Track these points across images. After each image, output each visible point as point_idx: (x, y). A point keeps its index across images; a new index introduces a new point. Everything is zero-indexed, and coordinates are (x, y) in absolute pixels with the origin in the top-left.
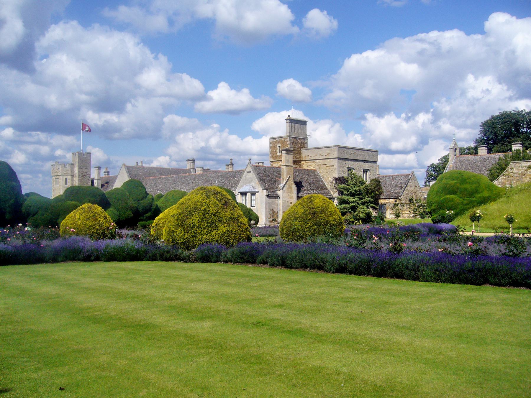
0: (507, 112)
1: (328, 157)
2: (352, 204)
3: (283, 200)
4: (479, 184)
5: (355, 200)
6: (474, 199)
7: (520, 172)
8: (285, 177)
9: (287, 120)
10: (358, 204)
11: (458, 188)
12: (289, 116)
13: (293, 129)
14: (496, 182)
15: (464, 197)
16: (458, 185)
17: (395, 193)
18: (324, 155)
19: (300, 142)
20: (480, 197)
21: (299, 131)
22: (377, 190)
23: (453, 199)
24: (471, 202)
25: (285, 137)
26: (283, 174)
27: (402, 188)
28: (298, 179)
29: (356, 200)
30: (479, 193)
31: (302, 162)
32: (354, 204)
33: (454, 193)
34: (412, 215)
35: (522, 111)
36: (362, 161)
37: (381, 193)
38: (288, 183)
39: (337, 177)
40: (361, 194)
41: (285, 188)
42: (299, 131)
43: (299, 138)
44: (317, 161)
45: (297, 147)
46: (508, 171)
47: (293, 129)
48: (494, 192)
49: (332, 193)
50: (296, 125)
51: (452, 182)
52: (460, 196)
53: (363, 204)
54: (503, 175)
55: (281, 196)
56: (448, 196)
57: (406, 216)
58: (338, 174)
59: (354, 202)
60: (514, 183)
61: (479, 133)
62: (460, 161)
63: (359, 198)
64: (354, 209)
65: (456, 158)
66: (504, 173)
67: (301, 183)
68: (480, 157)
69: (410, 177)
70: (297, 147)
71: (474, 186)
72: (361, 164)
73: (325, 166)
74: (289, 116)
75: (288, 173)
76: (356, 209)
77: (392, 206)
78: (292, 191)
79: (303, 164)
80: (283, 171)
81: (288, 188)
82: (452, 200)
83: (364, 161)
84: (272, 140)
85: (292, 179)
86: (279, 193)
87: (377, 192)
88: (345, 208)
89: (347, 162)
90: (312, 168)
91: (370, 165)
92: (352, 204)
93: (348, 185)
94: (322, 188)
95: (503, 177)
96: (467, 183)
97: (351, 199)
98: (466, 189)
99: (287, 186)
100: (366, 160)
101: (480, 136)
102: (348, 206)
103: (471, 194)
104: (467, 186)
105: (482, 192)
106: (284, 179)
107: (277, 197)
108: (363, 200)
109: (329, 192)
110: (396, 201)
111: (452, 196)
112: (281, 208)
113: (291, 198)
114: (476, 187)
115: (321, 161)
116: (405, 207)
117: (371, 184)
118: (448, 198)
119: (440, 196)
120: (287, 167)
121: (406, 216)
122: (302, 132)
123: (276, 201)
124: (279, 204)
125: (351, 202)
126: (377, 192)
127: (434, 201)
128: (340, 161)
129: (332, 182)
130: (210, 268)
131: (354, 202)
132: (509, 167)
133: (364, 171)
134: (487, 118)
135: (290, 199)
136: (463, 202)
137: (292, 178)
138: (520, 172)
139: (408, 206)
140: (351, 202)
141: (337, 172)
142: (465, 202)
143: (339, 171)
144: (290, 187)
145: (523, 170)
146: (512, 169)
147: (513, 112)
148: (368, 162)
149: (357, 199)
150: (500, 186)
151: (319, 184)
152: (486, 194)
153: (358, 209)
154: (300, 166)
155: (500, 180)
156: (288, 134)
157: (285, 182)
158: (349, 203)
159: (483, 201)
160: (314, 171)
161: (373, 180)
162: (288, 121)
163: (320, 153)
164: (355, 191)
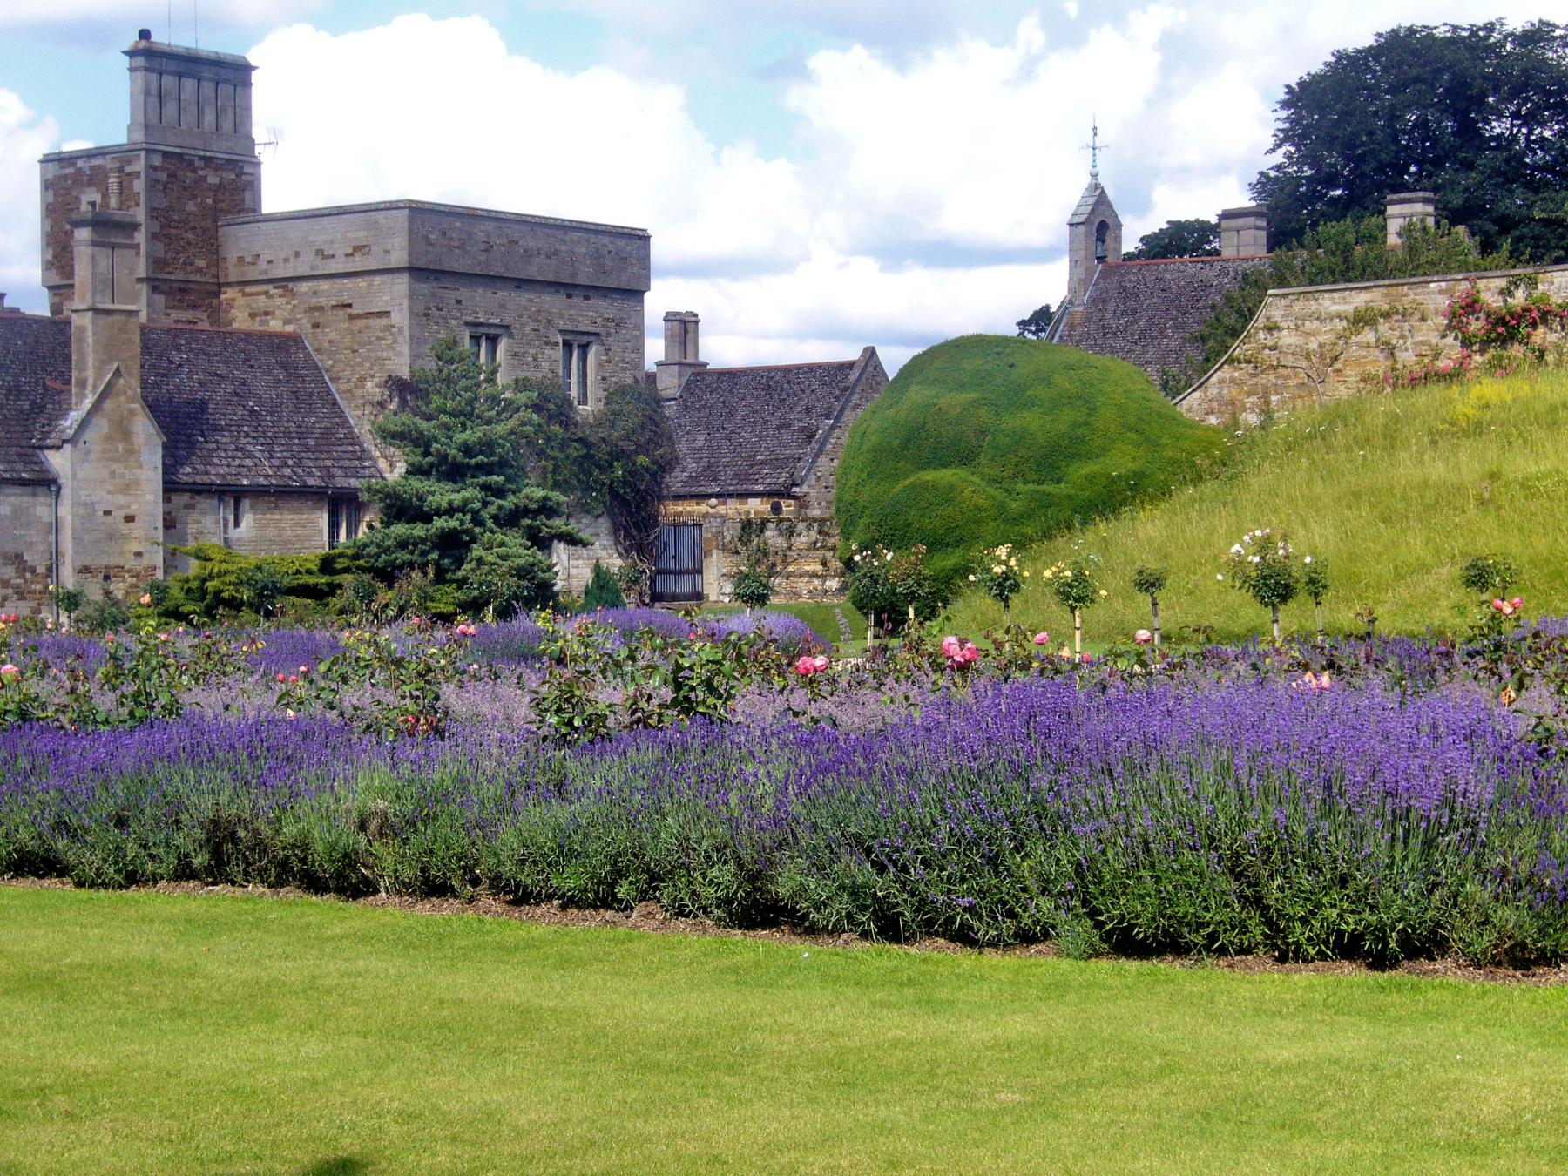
0: (1411, 31)
1: (358, 264)
2: (440, 523)
3: (76, 504)
4: (1093, 410)
5: (457, 498)
6: (1061, 489)
7: (1313, 345)
8: (90, 374)
9: (131, 54)
10: (477, 520)
11: (982, 433)
12: (145, 34)
13: (170, 109)
14: (1191, 403)
15: (1013, 478)
16: (985, 414)
17: (776, 464)
18: (341, 249)
19: (213, 180)
20: (1091, 479)
21: (209, 119)
22: (642, 449)
23: (952, 487)
24: (1048, 502)
25: (122, 154)
26: (82, 360)
27: (811, 437)
28: (186, 385)
29: (466, 502)
30: (1089, 456)
31: (228, 294)
32: (454, 523)
33: (966, 458)
34: (833, 584)
35: (1489, 28)
36: (556, 286)
37: (666, 466)
38: (108, 405)
39: (405, 374)
40: (502, 465)
41: (89, 435)
42: (209, 119)
43: (208, 161)
44: (304, 287)
45: (191, 207)
46: (1254, 341)
47: (170, 109)
48: (1168, 453)
49: (382, 464)
50: (189, 85)
51: (953, 401)
52: (995, 472)
53: (509, 520)
54: (1231, 361)
55: (65, 481)
56: (928, 476)
57: (803, 586)
58: (415, 357)
59: (451, 511)
60: (1283, 401)
61: (1270, 142)
62: (1124, 293)
63: (485, 487)
64: (453, 545)
65: (1103, 275)
66: (1239, 349)
67: (203, 406)
68: (1224, 272)
69: (853, 378)
70: (191, 207)
71: (1066, 419)
72: (551, 302)
73: (341, 313)
74: (145, 34)
75: (109, 349)
76: (467, 546)
77: (731, 532)
78: (130, 452)
79: (231, 304)
80: (82, 340)
81: (108, 438)
82: (948, 495)
83: (568, 288)
84: (53, 169)
85: (131, 384)
86: (58, 461)
87: (642, 459)
88: (402, 544)
89: (465, 293)
90: (275, 325)
91: (604, 308)
92: (440, 523)
93: (429, 418)
94: (327, 433)
95: (1227, 372)
96: (1030, 404)
97: (441, 494)
98: (1020, 437)
99: (101, 426)
100: (582, 280)
101: (1278, 157)
102: (419, 530)
103: (1050, 460)
104: (1031, 421)
105: (1103, 451)
106: (82, 384)
107: (46, 483)
108: (509, 503)
109: (363, 455)
110: (776, 509)
111: (947, 475)
112: (67, 546)
113: (126, 489)
114: (1075, 425)
115: (324, 285)
116: (801, 541)
117: (611, 416)
118: (926, 486)
119: (895, 477)
120: (103, 320)
121: (803, 586)
122: (227, 125)
123: (41, 509)
124: (57, 526)
125: (439, 513)
126: (642, 459)
127: (864, 498)
128: (425, 288)
129: (382, 405)
130: (1282, 1046)
131: (451, 511)
132: (1260, 320)
133: (568, 345)
134: (1313, 60)
135: (121, 499)
136: (1002, 507)
137: (135, 382)
138: (1313, 345)
139: (814, 534)
140: (439, 513)
141: (404, 349)
142: (1015, 506)
143: (415, 341)
144: (122, 431)
145: (1324, 334)
146: (1272, 328)
147: (1441, 32)
148: (590, 291)
149: (468, 493)
150: (1213, 420)
151: (311, 410)
152: (1121, 462)
153: (477, 551)
154: (215, 314)
155: (1212, 390)
156: (139, 136)
157: (88, 403)
158: (427, 519)
159: (1110, 500)
160: (285, 345)
161: (622, 391)
162: (140, 61)
163: (319, 239)
164: (467, 450)
